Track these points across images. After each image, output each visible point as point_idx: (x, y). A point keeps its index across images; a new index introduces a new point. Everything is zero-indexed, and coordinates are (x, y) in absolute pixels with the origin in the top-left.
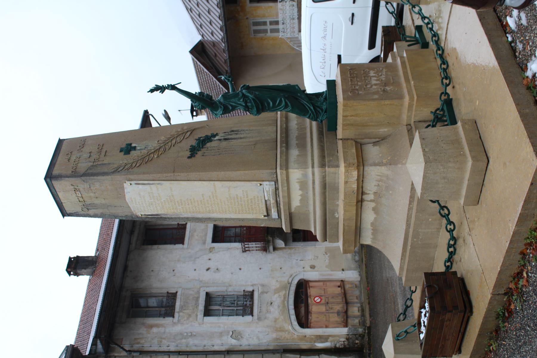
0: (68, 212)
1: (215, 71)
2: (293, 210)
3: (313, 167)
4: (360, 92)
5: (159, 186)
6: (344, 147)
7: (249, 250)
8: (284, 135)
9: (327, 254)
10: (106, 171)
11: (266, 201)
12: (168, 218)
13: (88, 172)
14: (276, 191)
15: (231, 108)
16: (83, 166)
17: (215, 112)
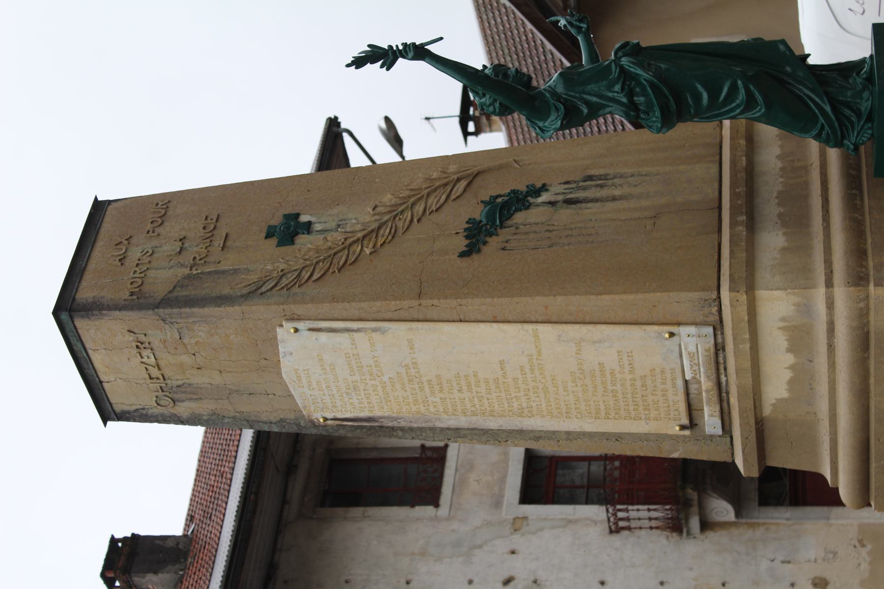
0: (118, 408)
2: (767, 411)
3: (829, 284)
5: (376, 336)
7: (629, 528)
8: (741, 190)
9: (863, 546)
10: (226, 291)
11: (686, 382)
12: (402, 429)
13: (175, 294)
14: (717, 355)
15: (585, 111)
16: (162, 278)
17: (541, 124)
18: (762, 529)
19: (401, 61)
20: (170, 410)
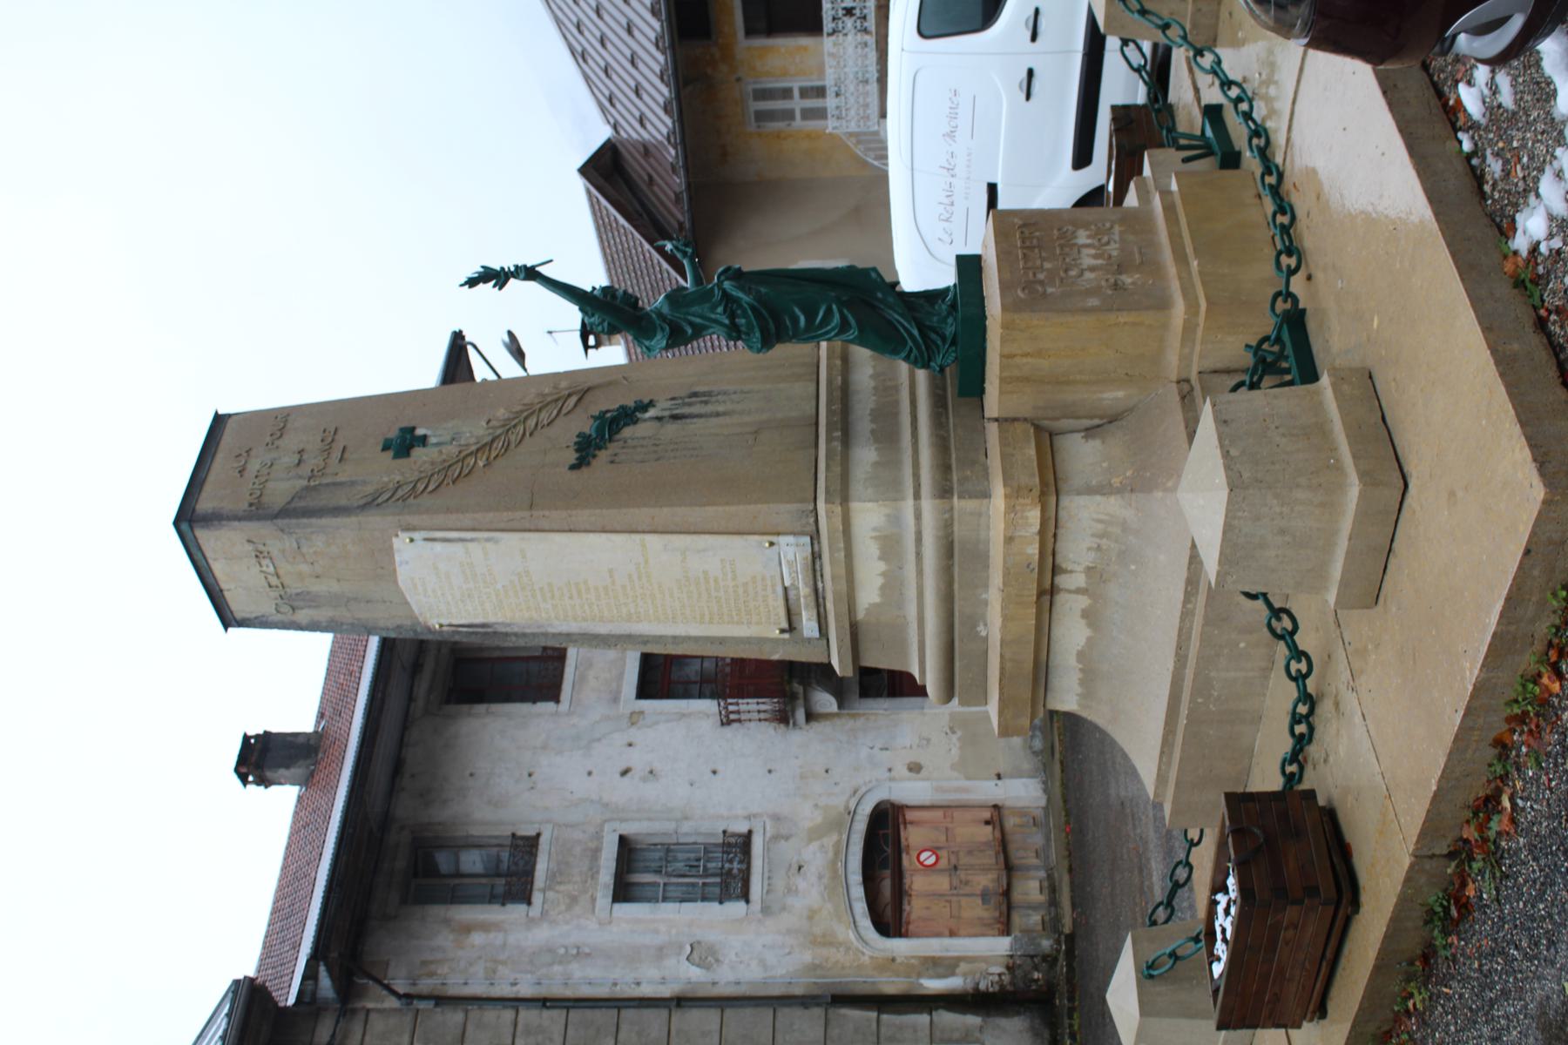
0: (239, 616)
1: (651, 226)
2: (861, 615)
3: (917, 496)
4: (1050, 290)
5: (488, 545)
6: (1004, 442)
7: (739, 721)
8: (837, 407)
10: (343, 502)
15: (690, 331)
16: (280, 490)
18: (862, 719)
19: (512, 281)
20: (289, 617)
